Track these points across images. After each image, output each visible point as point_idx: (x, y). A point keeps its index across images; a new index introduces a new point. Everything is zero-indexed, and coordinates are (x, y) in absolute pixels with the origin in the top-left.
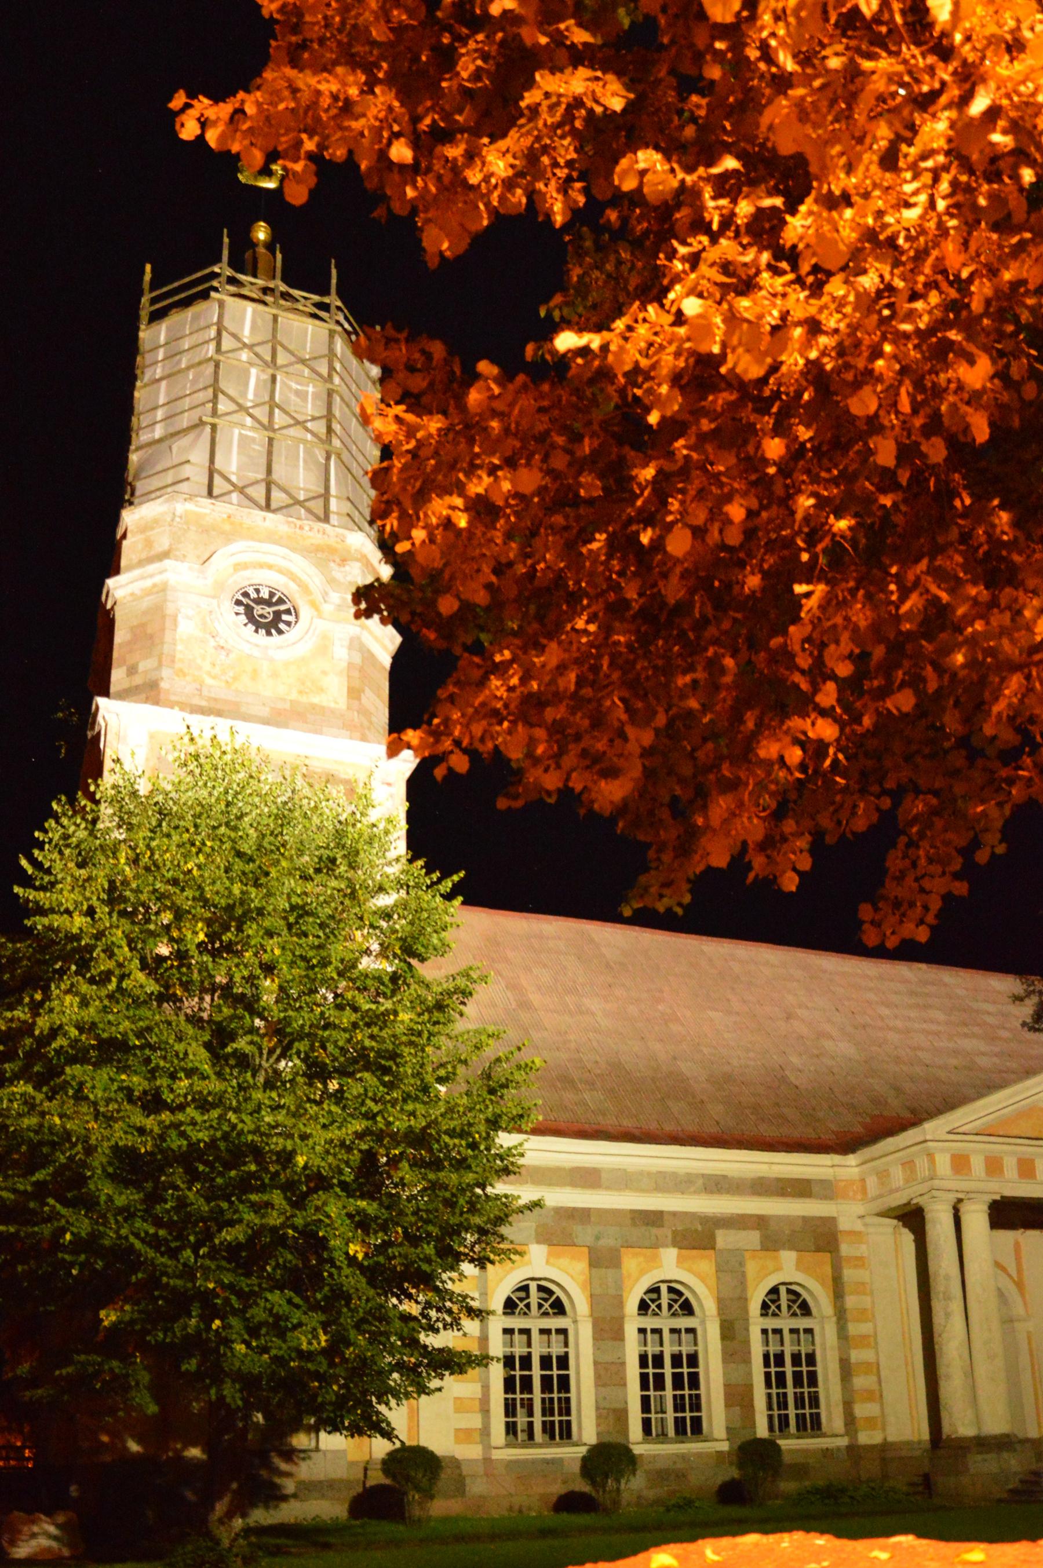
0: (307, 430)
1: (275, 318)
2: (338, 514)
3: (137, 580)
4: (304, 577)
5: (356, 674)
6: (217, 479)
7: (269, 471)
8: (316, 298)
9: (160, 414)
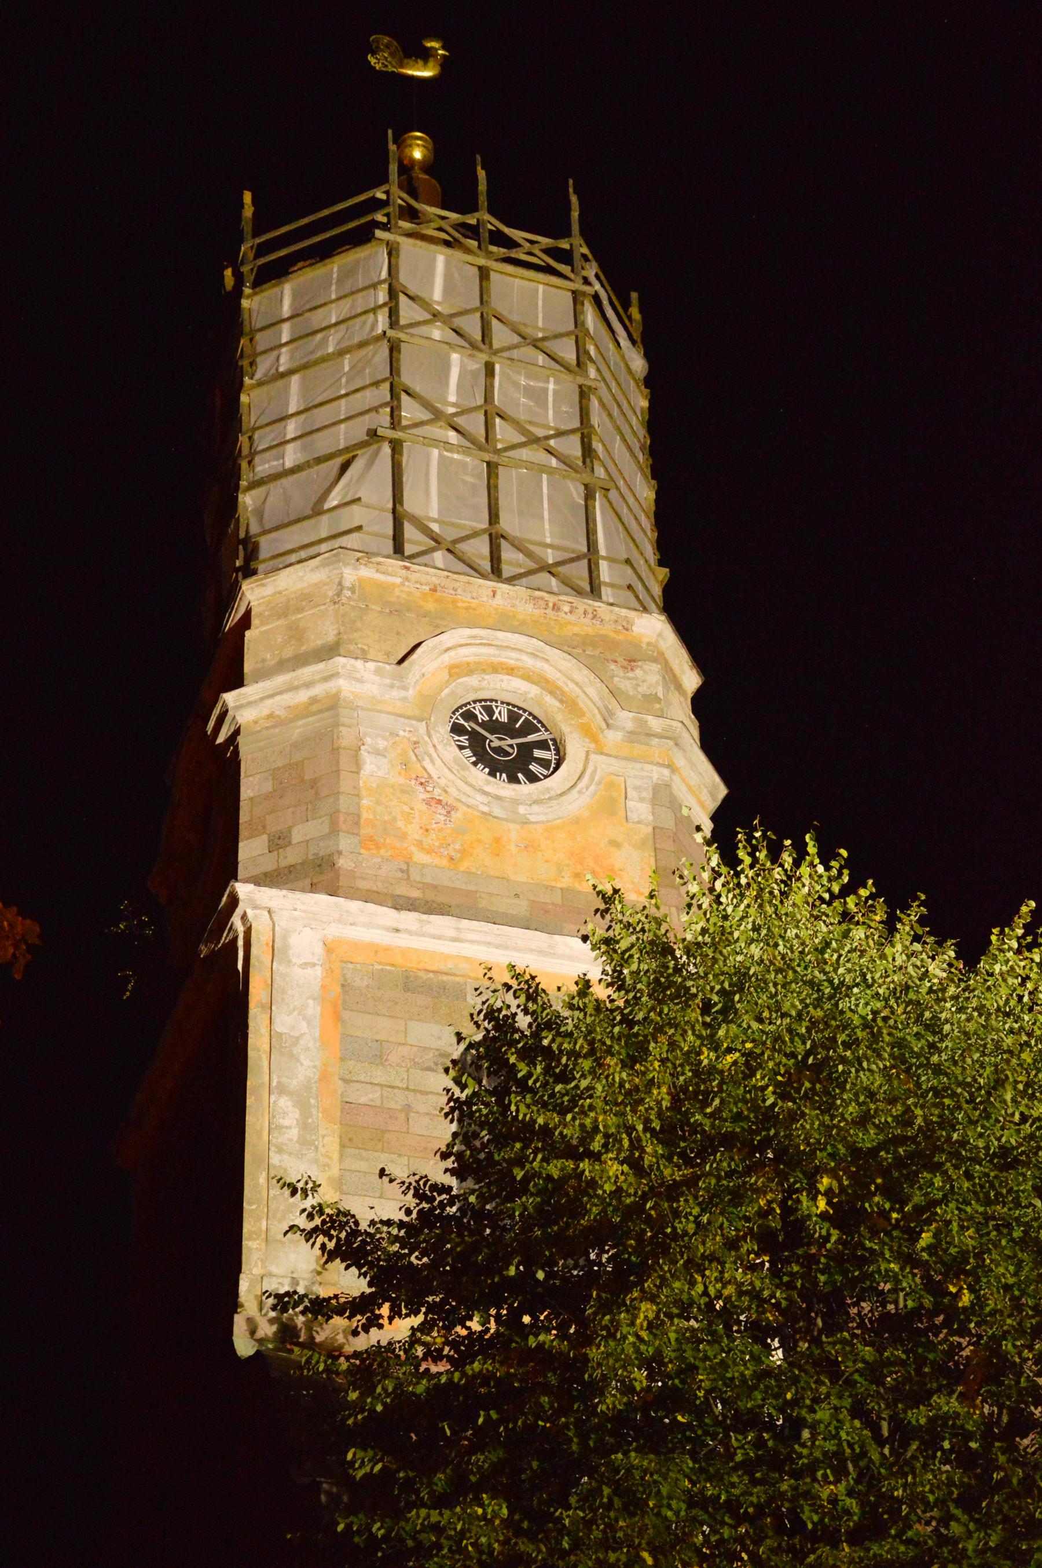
0: (549, 451)
1: (484, 274)
2: (612, 585)
3: (281, 693)
4: (570, 688)
5: (668, 845)
6: (410, 531)
7: (494, 516)
8: (545, 241)
9: (292, 429)
